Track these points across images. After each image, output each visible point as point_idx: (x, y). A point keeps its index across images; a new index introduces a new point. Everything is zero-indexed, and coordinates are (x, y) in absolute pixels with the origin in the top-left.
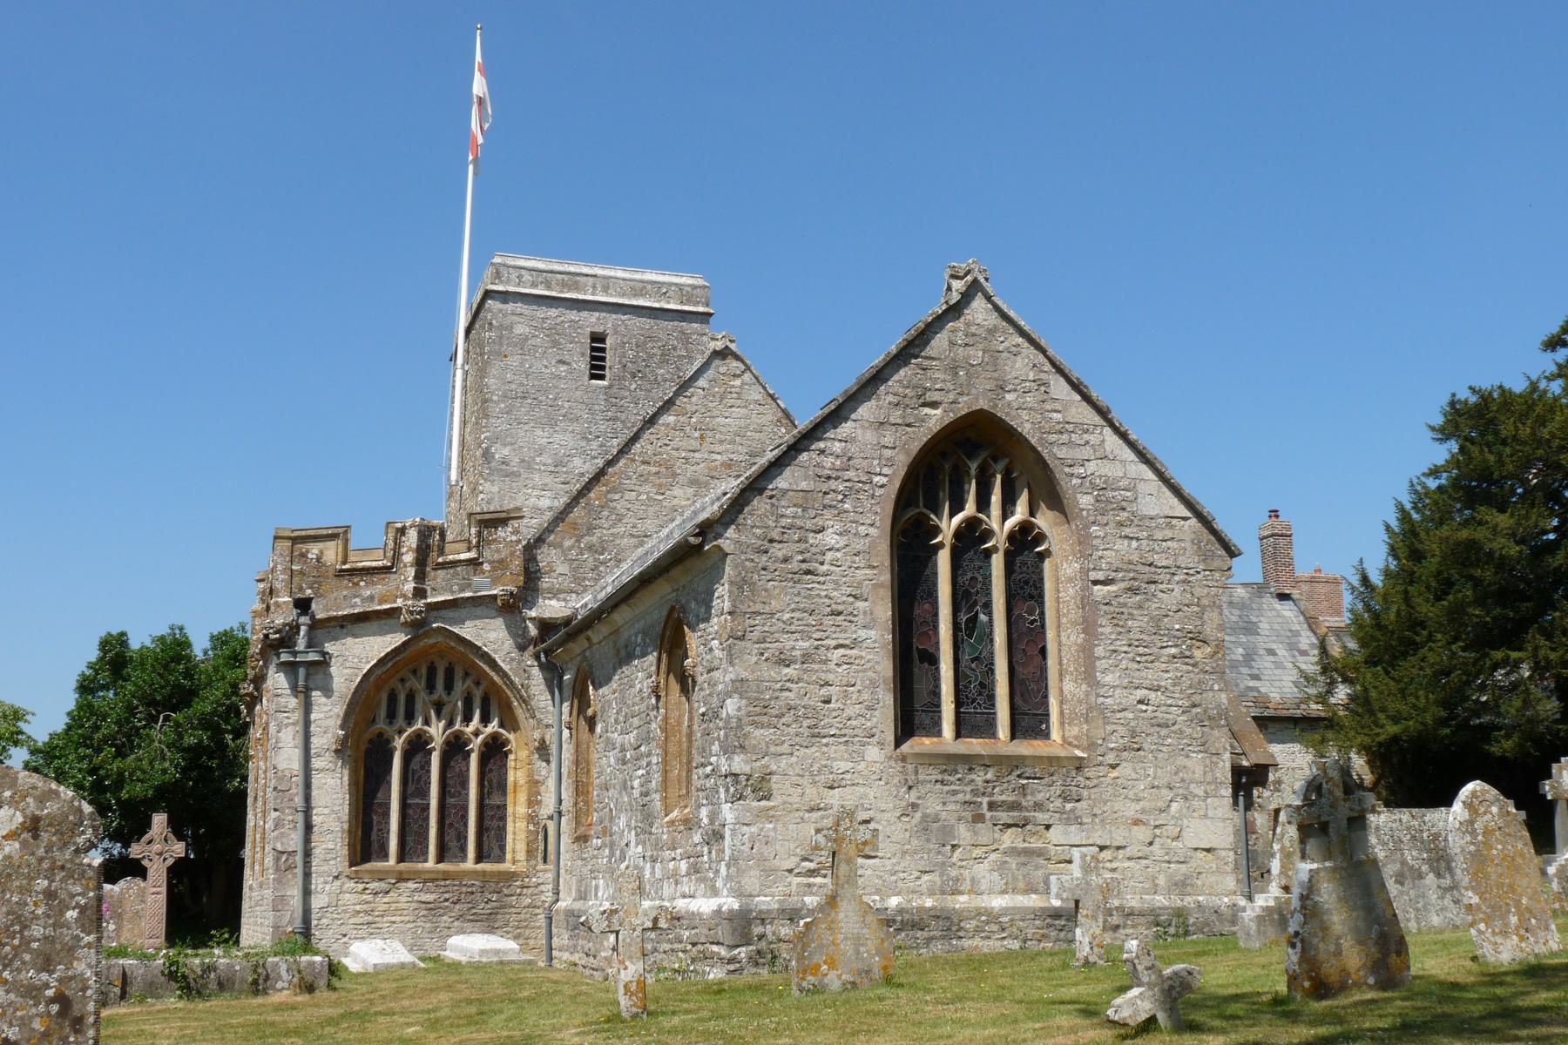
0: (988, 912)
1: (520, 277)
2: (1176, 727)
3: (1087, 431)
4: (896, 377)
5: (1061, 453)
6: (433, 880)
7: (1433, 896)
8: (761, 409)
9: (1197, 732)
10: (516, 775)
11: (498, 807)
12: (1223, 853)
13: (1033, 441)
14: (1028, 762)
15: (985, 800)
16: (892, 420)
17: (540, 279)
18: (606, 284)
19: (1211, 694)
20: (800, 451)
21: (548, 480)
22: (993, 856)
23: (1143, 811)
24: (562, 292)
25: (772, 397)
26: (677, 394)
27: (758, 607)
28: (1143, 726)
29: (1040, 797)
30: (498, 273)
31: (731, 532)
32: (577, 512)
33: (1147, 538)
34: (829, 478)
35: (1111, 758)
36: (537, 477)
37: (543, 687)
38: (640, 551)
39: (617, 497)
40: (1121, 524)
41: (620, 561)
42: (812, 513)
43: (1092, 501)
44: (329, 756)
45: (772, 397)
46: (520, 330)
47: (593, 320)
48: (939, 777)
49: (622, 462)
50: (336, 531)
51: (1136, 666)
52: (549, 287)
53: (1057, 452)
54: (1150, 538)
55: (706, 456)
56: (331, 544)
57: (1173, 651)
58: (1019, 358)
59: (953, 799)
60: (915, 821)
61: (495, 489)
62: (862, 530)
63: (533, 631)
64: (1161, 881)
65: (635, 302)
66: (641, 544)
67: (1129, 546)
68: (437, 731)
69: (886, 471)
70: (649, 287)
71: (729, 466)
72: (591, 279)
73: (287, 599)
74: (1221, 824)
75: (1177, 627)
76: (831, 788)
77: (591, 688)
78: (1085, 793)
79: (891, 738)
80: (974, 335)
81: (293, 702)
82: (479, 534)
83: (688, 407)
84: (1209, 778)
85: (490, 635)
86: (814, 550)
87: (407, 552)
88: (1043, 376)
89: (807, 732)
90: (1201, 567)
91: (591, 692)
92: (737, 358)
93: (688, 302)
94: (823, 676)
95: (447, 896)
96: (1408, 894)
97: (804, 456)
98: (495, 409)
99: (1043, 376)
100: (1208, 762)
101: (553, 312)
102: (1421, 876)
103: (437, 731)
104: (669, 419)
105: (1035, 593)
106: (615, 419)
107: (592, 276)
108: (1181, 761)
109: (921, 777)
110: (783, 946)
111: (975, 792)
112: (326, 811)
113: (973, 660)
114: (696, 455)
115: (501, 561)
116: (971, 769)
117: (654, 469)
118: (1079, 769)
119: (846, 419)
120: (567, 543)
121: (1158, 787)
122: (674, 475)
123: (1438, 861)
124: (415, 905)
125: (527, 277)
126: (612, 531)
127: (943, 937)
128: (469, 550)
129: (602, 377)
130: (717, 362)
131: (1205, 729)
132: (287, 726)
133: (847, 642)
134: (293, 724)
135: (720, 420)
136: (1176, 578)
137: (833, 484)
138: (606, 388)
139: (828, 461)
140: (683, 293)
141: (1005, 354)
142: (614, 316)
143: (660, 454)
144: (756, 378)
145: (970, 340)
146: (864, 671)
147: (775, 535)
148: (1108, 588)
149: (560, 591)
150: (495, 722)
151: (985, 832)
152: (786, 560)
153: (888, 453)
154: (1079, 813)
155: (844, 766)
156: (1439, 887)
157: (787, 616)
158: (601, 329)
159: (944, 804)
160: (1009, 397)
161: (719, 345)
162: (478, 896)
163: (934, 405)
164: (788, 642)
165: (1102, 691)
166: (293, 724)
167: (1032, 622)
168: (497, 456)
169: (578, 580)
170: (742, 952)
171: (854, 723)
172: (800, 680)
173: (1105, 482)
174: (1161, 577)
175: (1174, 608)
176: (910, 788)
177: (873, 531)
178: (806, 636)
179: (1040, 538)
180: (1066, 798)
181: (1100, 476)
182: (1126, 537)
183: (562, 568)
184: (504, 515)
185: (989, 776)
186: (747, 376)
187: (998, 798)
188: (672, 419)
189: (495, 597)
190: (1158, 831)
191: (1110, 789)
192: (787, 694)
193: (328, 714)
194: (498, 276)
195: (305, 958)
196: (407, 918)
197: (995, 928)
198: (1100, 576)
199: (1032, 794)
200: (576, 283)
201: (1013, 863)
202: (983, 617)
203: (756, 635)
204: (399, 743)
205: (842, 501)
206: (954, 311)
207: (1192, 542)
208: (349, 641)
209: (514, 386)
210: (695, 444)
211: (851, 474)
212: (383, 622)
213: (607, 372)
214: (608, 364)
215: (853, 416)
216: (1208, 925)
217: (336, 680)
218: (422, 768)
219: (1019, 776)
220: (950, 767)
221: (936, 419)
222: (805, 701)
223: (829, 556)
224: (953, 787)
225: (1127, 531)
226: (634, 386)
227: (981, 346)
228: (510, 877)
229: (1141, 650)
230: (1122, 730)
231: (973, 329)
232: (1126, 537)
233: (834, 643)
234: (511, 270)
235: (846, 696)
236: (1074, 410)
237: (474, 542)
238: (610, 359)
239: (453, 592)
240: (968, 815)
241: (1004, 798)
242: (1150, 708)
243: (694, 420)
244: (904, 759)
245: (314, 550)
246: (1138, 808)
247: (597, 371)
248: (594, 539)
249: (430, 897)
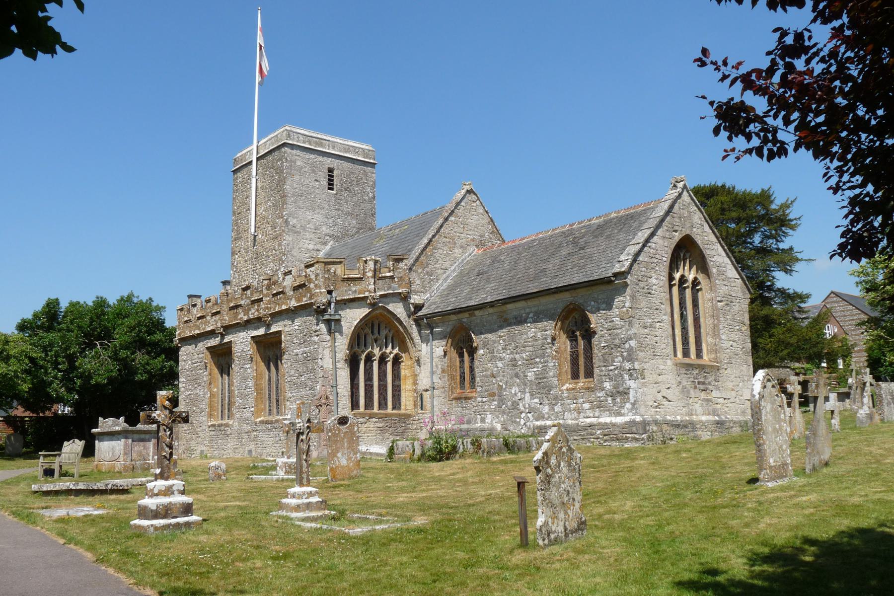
0: (701, 422)
1: (298, 138)
6: (382, 418)
10: (404, 372)
11: (398, 386)
13: (701, 247)
17: (307, 140)
18: (334, 145)
21: (312, 236)
23: (734, 386)
24: (315, 147)
25: (486, 212)
26: (455, 208)
32: (423, 257)
36: (308, 234)
37: (417, 334)
38: (445, 276)
39: (436, 251)
41: (438, 280)
44: (342, 362)
45: (486, 212)
46: (299, 163)
47: (329, 162)
49: (437, 236)
50: (341, 260)
51: (729, 333)
54: (730, 286)
55: (465, 235)
56: (339, 266)
61: (290, 239)
63: (412, 309)
66: (445, 273)
68: (377, 352)
70: (351, 148)
72: (328, 142)
73: (324, 290)
77: (473, 335)
78: (720, 379)
81: (328, 337)
82: (393, 265)
85: (398, 309)
87: (369, 271)
89: (652, 354)
90: (743, 297)
91: (473, 337)
92: (475, 194)
93: (367, 157)
95: (387, 424)
98: (290, 200)
99: (702, 222)
101: (312, 156)
103: (377, 352)
104: (452, 218)
106: (338, 209)
107: (328, 140)
112: (343, 387)
114: (462, 235)
115: (401, 277)
117: (448, 240)
118: (718, 370)
120: (420, 271)
122: (455, 243)
124: (376, 429)
125: (301, 138)
126: (435, 266)
127: (692, 431)
128: (389, 272)
132: (326, 348)
134: (329, 347)
140: (365, 153)
142: (337, 161)
143: (450, 234)
144: (481, 203)
145: (684, 207)
147: (640, 278)
149: (418, 292)
150: (397, 349)
152: (643, 288)
157: (645, 310)
160: (694, 230)
161: (468, 188)
162: (398, 424)
163: (676, 231)
166: (329, 347)
168: (291, 223)
169: (424, 287)
170: (644, 436)
179: (699, 283)
183: (418, 282)
184: (401, 257)
185: (697, 372)
188: (453, 218)
189: (400, 293)
193: (342, 343)
194: (289, 136)
195: (539, 438)
196: (373, 434)
197: (704, 427)
198: (719, 299)
200: (321, 143)
202: (685, 312)
203: (637, 317)
204: (363, 356)
208: (348, 310)
209: (297, 190)
212: (360, 302)
213: (335, 187)
214: (335, 183)
217: (344, 328)
218: (370, 368)
226: (346, 195)
228: (408, 416)
233: (657, 321)
234: (295, 134)
237: (392, 268)
238: (336, 181)
239: (385, 290)
240: (693, 386)
243: (461, 220)
245: (333, 268)
248: (429, 269)
249: (381, 425)
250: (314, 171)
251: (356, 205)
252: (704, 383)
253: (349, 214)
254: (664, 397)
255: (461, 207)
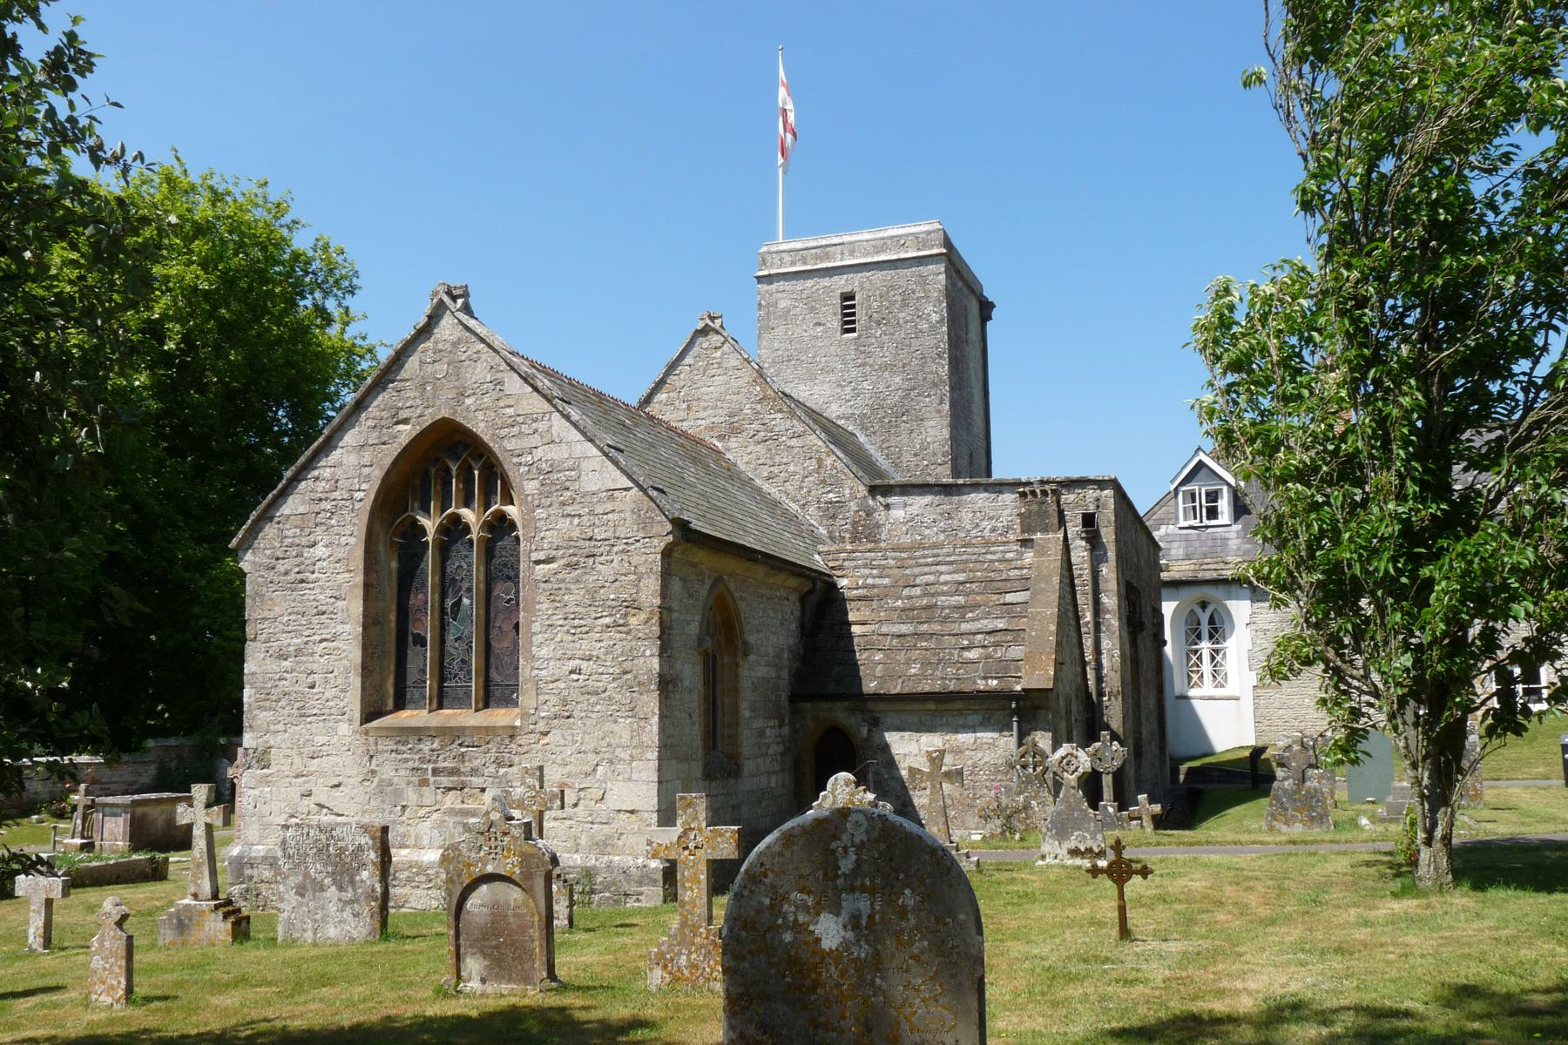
0: (418, 865)
2: (607, 693)
3: (536, 420)
4: (375, 403)
5: (510, 445)
7: (332, 909)
8: (739, 373)
9: (625, 698)
12: (646, 815)
14: (467, 733)
15: (431, 766)
16: (370, 442)
18: (852, 248)
19: (642, 660)
20: (300, 481)
22: (435, 816)
27: (266, 614)
28: (575, 695)
29: (476, 763)
30: (764, 260)
31: (249, 556)
33: (589, 514)
34: (320, 500)
35: (541, 726)
40: (563, 504)
42: (307, 531)
43: (538, 485)
46: (782, 304)
48: (394, 748)
52: (805, 263)
53: (505, 446)
54: (591, 513)
57: (607, 620)
58: (479, 364)
59: (405, 766)
60: (374, 785)
62: (343, 540)
64: (583, 841)
65: (876, 259)
67: (571, 523)
69: (364, 486)
70: (889, 242)
71: (712, 429)
74: (644, 787)
75: (612, 597)
76: (312, 758)
78: (516, 759)
79: (357, 715)
80: (440, 351)
83: (677, 384)
84: (636, 741)
86: (307, 562)
88: (499, 375)
93: (925, 247)
94: (309, 666)
96: (307, 905)
97: (303, 485)
99: (499, 375)
100: (635, 726)
101: (809, 283)
102: (322, 889)
105: (512, 574)
106: (863, 365)
108: (609, 726)
109: (380, 748)
110: (264, 886)
111: (422, 760)
113: (456, 640)
116: (420, 740)
118: (512, 737)
119: (336, 448)
121: (584, 752)
123: (342, 874)
125: (787, 258)
129: (853, 330)
130: (701, 339)
131: (634, 695)
133: (329, 636)
135: (705, 390)
136: (615, 549)
137: (324, 505)
138: (855, 339)
139: (321, 485)
141: (467, 363)
146: (341, 660)
148: (551, 566)
151: (429, 795)
152: (286, 574)
153: (366, 471)
154: (509, 777)
155: (321, 739)
156: (340, 900)
158: (847, 289)
159: (397, 770)
160: (468, 401)
163: (405, 421)
164: (285, 639)
165: (537, 664)
167: (508, 601)
171: (330, 703)
172: (293, 671)
173: (551, 466)
174: (601, 549)
175: (611, 579)
176: (372, 757)
177: (352, 540)
178: (299, 634)
180: (499, 763)
181: (547, 461)
182: (568, 515)
185: (435, 746)
186: (726, 347)
187: (441, 765)
190: (582, 794)
191: (539, 754)
192: (283, 682)
197: (423, 878)
198: (541, 556)
199: (470, 760)
201: (451, 821)
205: (330, 518)
206: (424, 332)
207: (633, 512)
210: (683, 414)
211: (336, 494)
215: (341, 444)
216: (615, 884)
219: (460, 745)
220: (404, 738)
221: (406, 433)
222: (297, 688)
223: (319, 564)
224: (405, 756)
225: (569, 509)
227: (446, 360)
229: (576, 622)
230: (554, 700)
231: (440, 346)
232: (568, 515)
233: (318, 638)
235: (326, 681)
236: (525, 403)
238: (861, 315)
240: (415, 779)
241: (446, 764)
242: (582, 677)
244: (367, 733)
246: (565, 772)
247: (848, 325)
250: (812, 309)
251: (900, 345)
252: (454, 772)
253: (884, 367)
254: (321, 806)
255: (683, 369)
